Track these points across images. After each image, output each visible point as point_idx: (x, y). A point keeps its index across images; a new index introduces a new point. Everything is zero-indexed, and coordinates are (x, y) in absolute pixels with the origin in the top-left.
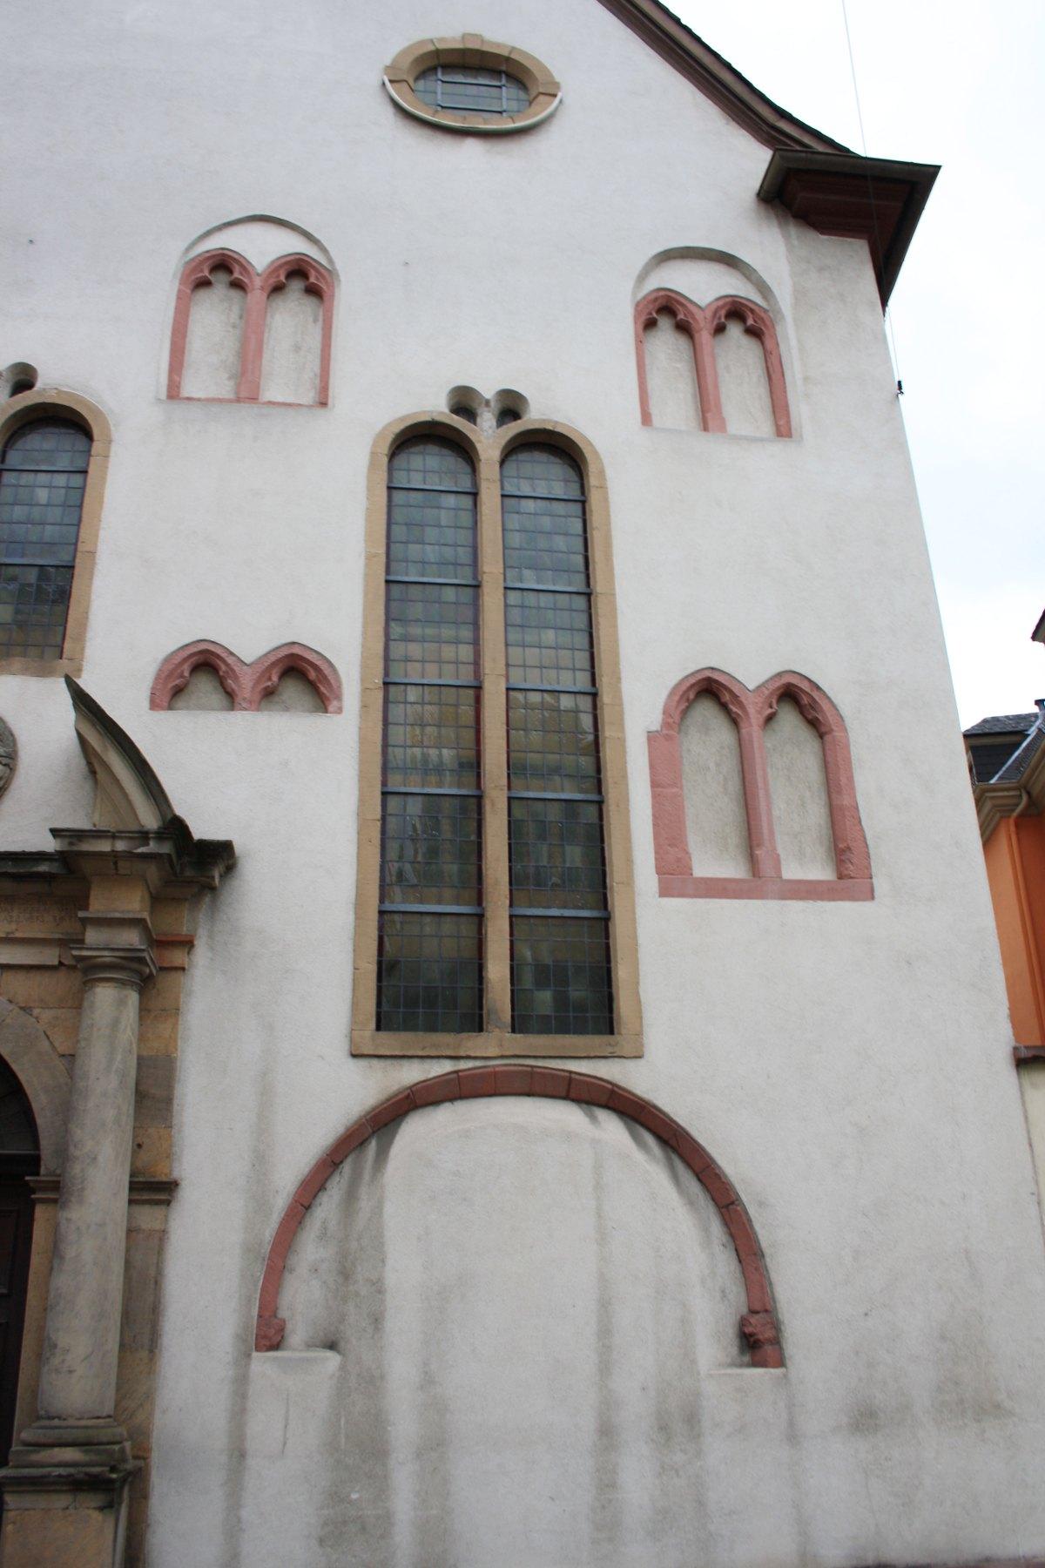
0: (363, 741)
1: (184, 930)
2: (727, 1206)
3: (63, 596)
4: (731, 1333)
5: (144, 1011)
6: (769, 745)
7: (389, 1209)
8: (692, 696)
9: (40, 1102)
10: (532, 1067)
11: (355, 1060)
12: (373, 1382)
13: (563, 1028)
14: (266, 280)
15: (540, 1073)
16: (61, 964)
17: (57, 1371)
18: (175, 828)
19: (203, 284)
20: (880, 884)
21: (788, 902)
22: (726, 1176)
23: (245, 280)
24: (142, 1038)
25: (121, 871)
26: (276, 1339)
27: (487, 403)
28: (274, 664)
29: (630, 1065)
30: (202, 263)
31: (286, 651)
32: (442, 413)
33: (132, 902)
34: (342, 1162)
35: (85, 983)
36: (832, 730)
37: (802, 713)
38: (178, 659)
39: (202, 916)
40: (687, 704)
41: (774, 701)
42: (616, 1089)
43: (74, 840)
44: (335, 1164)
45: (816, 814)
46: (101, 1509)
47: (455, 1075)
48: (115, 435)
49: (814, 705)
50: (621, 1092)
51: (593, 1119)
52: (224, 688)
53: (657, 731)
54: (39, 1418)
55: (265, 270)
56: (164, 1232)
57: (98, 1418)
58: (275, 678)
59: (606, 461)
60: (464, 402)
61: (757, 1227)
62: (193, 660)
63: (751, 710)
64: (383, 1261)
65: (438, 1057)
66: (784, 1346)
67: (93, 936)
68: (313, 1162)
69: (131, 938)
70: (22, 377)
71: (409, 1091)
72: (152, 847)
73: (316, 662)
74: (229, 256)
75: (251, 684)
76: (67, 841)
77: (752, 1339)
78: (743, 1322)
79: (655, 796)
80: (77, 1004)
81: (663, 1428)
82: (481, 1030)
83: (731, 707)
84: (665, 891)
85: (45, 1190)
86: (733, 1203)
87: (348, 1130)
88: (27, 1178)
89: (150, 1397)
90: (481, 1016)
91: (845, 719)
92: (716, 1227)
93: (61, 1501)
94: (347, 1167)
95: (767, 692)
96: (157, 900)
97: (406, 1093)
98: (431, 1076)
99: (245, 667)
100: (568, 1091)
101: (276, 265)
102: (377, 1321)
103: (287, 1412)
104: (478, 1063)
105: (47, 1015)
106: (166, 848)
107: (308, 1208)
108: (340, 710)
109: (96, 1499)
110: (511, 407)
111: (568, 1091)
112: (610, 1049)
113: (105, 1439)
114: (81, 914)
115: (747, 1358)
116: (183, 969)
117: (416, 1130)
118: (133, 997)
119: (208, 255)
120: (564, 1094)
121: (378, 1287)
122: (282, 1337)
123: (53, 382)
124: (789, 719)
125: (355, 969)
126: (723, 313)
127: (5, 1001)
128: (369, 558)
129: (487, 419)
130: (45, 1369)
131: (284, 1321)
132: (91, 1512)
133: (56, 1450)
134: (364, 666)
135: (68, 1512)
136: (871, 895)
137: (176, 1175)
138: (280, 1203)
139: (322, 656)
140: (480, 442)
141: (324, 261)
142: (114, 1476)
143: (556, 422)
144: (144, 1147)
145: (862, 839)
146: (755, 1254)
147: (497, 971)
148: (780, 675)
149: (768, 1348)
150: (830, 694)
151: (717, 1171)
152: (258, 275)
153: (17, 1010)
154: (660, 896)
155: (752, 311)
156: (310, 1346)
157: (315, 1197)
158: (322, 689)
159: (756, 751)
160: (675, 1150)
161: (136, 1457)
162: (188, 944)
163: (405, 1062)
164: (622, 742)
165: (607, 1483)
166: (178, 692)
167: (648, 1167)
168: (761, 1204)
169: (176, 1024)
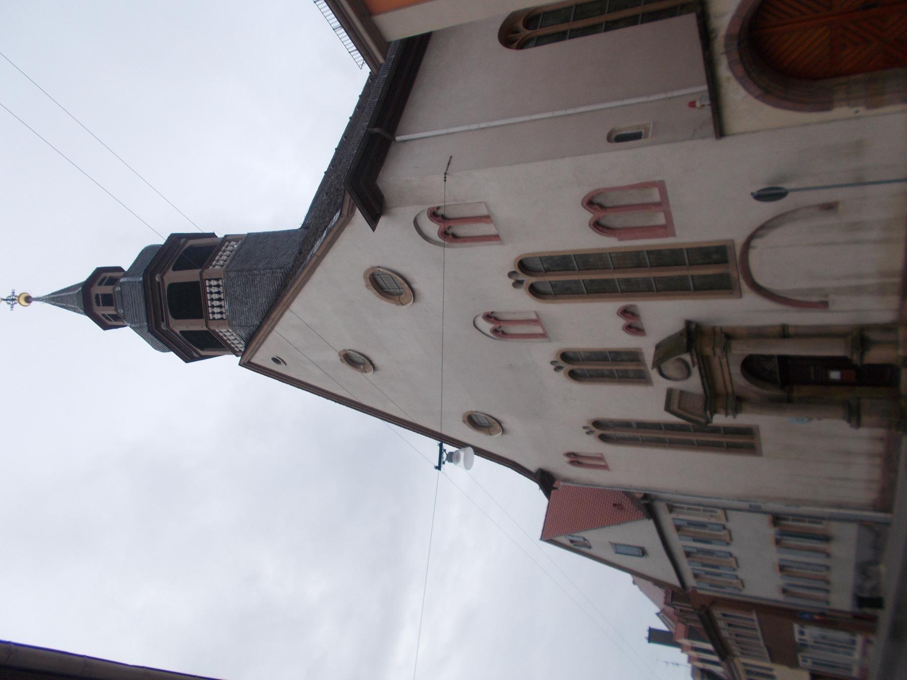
51: (754, 248)
84: (674, 235)
110: (511, 274)
126: (437, 219)
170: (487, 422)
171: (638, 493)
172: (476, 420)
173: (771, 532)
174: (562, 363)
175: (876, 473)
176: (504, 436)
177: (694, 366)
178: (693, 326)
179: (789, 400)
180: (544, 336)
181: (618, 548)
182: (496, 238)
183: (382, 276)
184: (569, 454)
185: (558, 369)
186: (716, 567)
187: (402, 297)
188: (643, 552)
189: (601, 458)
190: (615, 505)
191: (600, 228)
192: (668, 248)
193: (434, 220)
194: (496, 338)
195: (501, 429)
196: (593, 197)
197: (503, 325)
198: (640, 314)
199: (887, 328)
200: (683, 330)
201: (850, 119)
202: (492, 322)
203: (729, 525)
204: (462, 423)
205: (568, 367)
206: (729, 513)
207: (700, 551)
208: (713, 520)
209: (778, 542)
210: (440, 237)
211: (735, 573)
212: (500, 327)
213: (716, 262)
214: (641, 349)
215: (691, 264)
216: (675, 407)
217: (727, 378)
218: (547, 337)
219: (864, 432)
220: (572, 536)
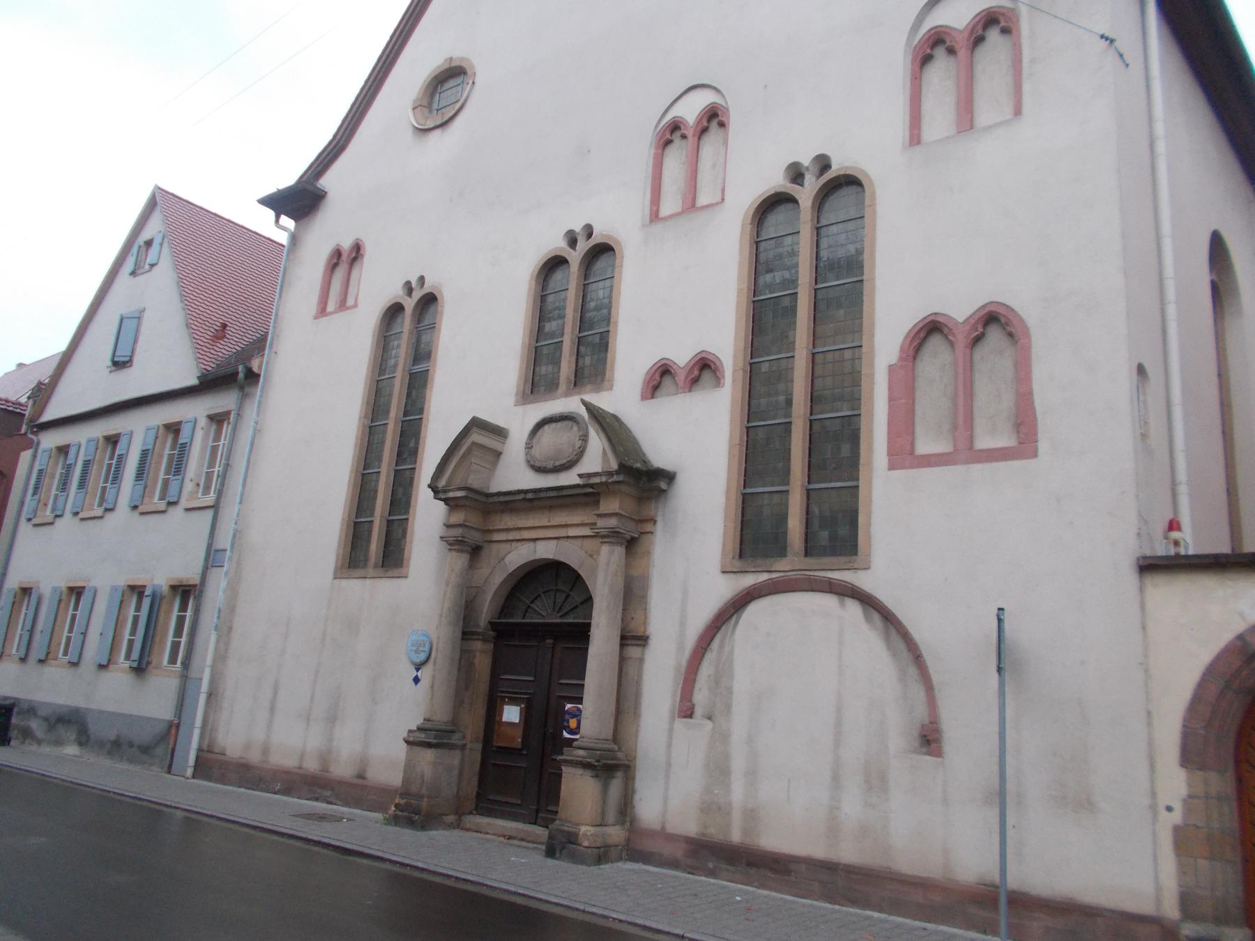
1: (652, 513)
14: (695, 130)
20: (1043, 446)
21: (972, 465)
27: (807, 168)
29: (861, 573)
30: (665, 131)
31: (699, 357)
45: (1007, 402)
51: (842, 604)
53: (895, 364)
55: (694, 123)
62: (660, 370)
72: (615, 478)
74: (678, 121)
76: (587, 479)
79: (890, 407)
84: (892, 467)
87: (719, 610)
104: (781, 574)
110: (823, 163)
115: (924, 750)
117: (754, 611)
119: (667, 125)
121: (730, 690)
126: (980, 27)
134: (735, 357)
137: (647, 633)
141: (724, 104)
148: (984, 307)
155: (1003, 14)
163: (747, 575)
170: (443, 104)
171: (262, 362)
172: (452, 83)
173: (160, 578)
174: (417, 295)
175: (285, 761)
176: (410, 130)
177: (580, 476)
178: (663, 485)
179: (467, 635)
180: (655, 216)
181: (129, 326)
182: (915, 138)
183: (460, 88)
184: (357, 249)
185: (409, 288)
186: (82, 484)
187: (426, 111)
188: (119, 365)
189: (343, 305)
190: (224, 326)
191: (922, 335)
192: (414, 493)
193: (978, 18)
194: (661, 125)
195: (426, 127)
196: (714, 372)
197: (691, 140)
198: (693, 393)
199: (626, 809)
200: (652, 466)
201: (1153, 795)
202: (699, 121)
203: (177, 513)
204: (447, 56)
205: (409, 304)
206: (209, 514)
207: (69, 469)
208: (189, 487)
209: (137, 591)
210: (931, 29)
211: (68, 514)
212: (684, 137)
213: (808, 537)
214: (611, 388)
215: (390, 523)
216: (477, 437)
217: (526, 534)
218: (651, 221)
219: (399, 751)
220: (161, 244)
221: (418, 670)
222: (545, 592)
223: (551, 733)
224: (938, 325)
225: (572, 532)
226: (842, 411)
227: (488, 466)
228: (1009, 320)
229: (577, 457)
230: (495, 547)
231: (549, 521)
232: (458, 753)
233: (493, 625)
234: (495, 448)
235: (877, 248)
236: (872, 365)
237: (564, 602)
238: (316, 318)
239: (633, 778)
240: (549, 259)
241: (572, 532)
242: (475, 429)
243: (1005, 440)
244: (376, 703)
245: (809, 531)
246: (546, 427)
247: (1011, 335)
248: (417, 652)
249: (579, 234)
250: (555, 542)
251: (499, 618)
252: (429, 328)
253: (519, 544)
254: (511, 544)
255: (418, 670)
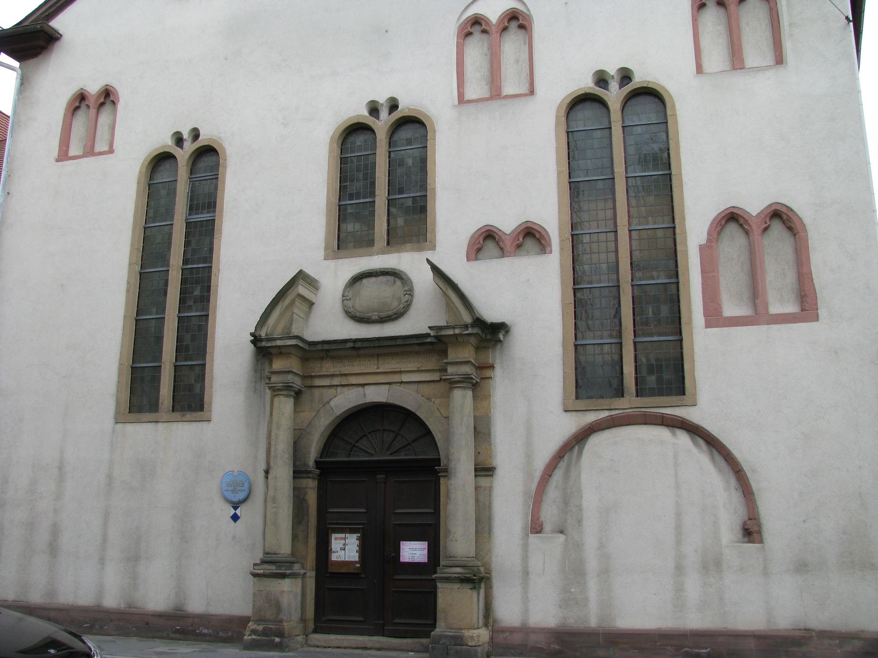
0: (562, 266)
1: (490, 361)
2: (738, 472)
3: (423, 209)
4: (738, 528)
5: (475, 397)
6: (766, 243)
7: (584, 476)
8: (723, 223)
9: (438, 436)
10: (645, 412)
11: (566, 413)
12: (579, 546)
13: (661, 394)
15: (648, 415)
16: (441, 379)
17: (452, 540)
18: (479, 322)
19: (469, 34)
20: (822, 312)
22: (736, 458)
23: (488, 29)
24: (475, 408)
25: (459, 341)
26: (539, 529)
27: (613, 76)
28: (519, 233)
29: (692, 409)
30: (466, 24)
32: (590, 88)
33: (466, 353)
34: (564, 456)
35: (450, 388)
36: (799, 232)
37: (784, 223)
38: (477, 235)
39: (497, 353)
40: (721, 227)
41: (768, 220)
42: (684, 420)
43: (438, 331)
44: (560, 457)
45: (791, 277)
46: (471, 589)
47: (610, 417)
48: (437, 128)
49: (789, 219)
50: (686, 421)
51: (674, 434)
52: (499, 246)
54: (447, 557)
55: (497, 22)
56: (491, 487)
57: (469, 557)
58: (521, 239)
59: (675, 100)
60: (601, 79)
61: (751, 482)
62: (484, 235)
63: (754, 227)
64: (581, 497)
65: (603, 410)
66: (763, 534)
67: (450, 369)
68: (550, 457)
69: (467, 369)
70: (393, 103)
71: (590, 425)
72: (470, 331)
73: (538, 230)
75: (510, 244)
76: (435, 331)
77: (748, 531)
78: (745, 524)
80: (447, 396)
81: (705, 568)
82: (623, 396)
83: (744, 226)
84: (708, 325)
85: (442, 472)
86: (740, 471)
88: (436, 468)
89: (490, 551)
90: (623, 389)
91: (806, 225)
92: (733, 482)
93: (456, 586)
94: (566, 457)
95: (763, 216)
96: (477, 349)
97: (589, 426)
98: (599, 418)
99: (507, 236)
100: (663, 422)
101: (502, 17)
102: (580, 522)
103: (544, 557)
105: (437, 401)
106: (476, 330)
107: (550, 476)
108: (551, 252)
109: (471, 586)
110: (626, 76)
111: (663, 422)
112: (680, 402)
113: (471, 565)
114: (445, 361)
115: (746, 539)
116: (491, 378)
117: (596, 441)
118: (469, 393)
120: (661, 423)
121: (580, 508)
122: (542, 528)
123: (407, 105)
124: (777, 227)
125: (564, 373)
127: (420, 396)
128: (559, 173)
129: (614, 85)
130: (448, 539)
131: (542, 522)
132: (468, 590)
133: (453, 568)
135: (459, 590)
136: (817, 319)
137: (494, 465)
138: (538, 474)
139: (541, 226)
140: (609, 100)
141: (525, 10)
142: (475, 578)
143: (649, 82)
144: (481, 453)
145: (813, 289)
146: (750, 493)
147: (629, 369)
148: (770, 205)
149: (755, 535)
150: (798, 213)
151: (732, 456)
152: (494, 25)
153: (426, 400)
154: (706, 328)
156: (553, 532)
157: (553, 471)
158: (542, 242)
159: (756, 249)
160: (714, 447)
161: (486, 573)
162: (492, 367)
163: (588, 413)
164: (686, 252)
165: (679, 589)
166: (479, 250)
167: (699, 455)
168: (753, 471)
169: (490, 402)
184: (108, 96)
216: (302, 289)
217: (354, 380)
221: (235, 508)
222: (369, 433)
223: (393, 556)
224: (735, 215)
225: (405, 378)
226: (658, 278)
227: (302, 316)
228: (790, 218)
229: (404, 309)
230: (316, 392)
231: (378, 368)
232: (299, 581)
233: (317, 463)
234: (311, 300)
235: (681, 150)
236: (685, 244)
237: (393, 440)
238: (57, 161)
239: (491, 587)
240: (353, 124)
241: (405, 378)
242: (301, 282)
243: (791, 308)
244: (187, 542)
245: (638, 375)
246: (365, 281)
247: (790, 229)
248: (234, 491)
249: (382, 105)
250: (387, 386)
251: (321, 458)
252: (204, 180)
253: (346, 389)
254: (336, 390)
255: (235, 508)
